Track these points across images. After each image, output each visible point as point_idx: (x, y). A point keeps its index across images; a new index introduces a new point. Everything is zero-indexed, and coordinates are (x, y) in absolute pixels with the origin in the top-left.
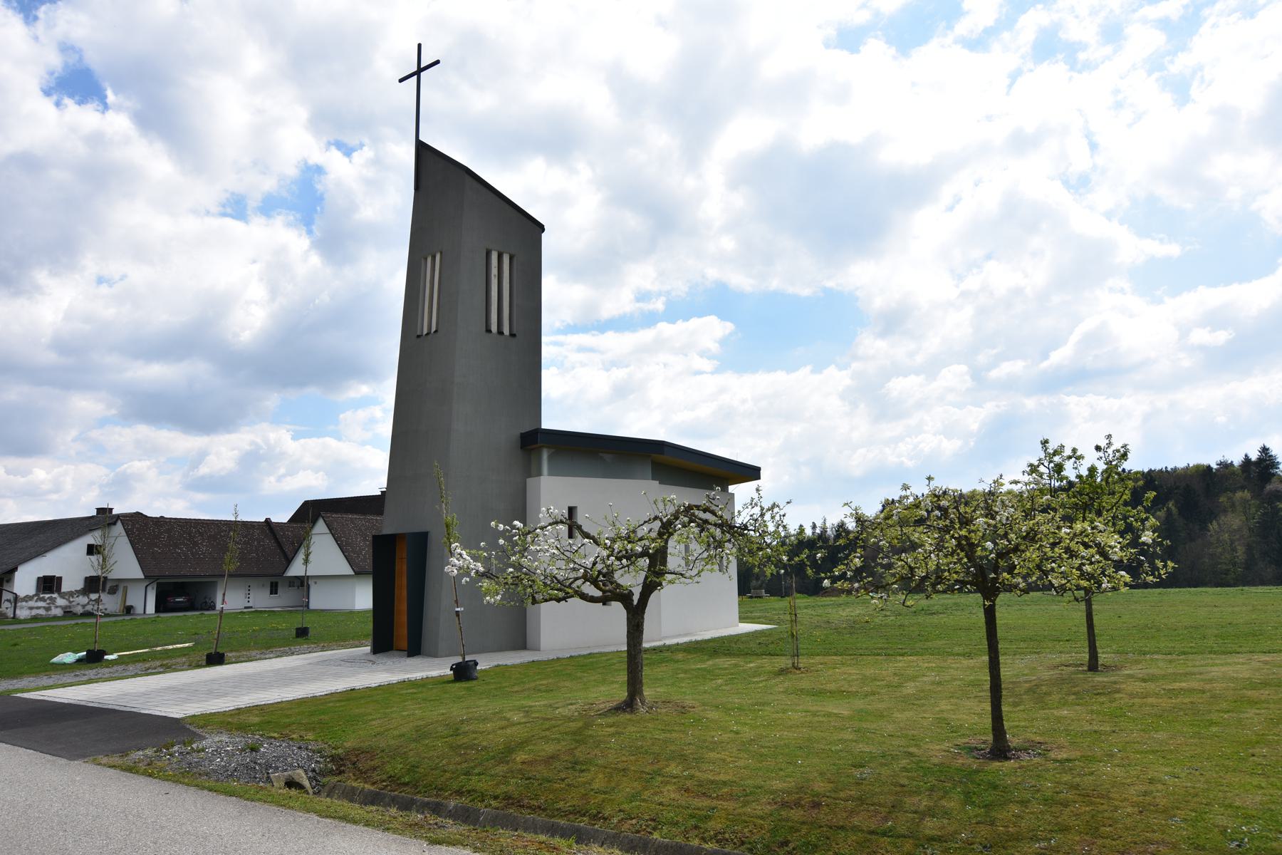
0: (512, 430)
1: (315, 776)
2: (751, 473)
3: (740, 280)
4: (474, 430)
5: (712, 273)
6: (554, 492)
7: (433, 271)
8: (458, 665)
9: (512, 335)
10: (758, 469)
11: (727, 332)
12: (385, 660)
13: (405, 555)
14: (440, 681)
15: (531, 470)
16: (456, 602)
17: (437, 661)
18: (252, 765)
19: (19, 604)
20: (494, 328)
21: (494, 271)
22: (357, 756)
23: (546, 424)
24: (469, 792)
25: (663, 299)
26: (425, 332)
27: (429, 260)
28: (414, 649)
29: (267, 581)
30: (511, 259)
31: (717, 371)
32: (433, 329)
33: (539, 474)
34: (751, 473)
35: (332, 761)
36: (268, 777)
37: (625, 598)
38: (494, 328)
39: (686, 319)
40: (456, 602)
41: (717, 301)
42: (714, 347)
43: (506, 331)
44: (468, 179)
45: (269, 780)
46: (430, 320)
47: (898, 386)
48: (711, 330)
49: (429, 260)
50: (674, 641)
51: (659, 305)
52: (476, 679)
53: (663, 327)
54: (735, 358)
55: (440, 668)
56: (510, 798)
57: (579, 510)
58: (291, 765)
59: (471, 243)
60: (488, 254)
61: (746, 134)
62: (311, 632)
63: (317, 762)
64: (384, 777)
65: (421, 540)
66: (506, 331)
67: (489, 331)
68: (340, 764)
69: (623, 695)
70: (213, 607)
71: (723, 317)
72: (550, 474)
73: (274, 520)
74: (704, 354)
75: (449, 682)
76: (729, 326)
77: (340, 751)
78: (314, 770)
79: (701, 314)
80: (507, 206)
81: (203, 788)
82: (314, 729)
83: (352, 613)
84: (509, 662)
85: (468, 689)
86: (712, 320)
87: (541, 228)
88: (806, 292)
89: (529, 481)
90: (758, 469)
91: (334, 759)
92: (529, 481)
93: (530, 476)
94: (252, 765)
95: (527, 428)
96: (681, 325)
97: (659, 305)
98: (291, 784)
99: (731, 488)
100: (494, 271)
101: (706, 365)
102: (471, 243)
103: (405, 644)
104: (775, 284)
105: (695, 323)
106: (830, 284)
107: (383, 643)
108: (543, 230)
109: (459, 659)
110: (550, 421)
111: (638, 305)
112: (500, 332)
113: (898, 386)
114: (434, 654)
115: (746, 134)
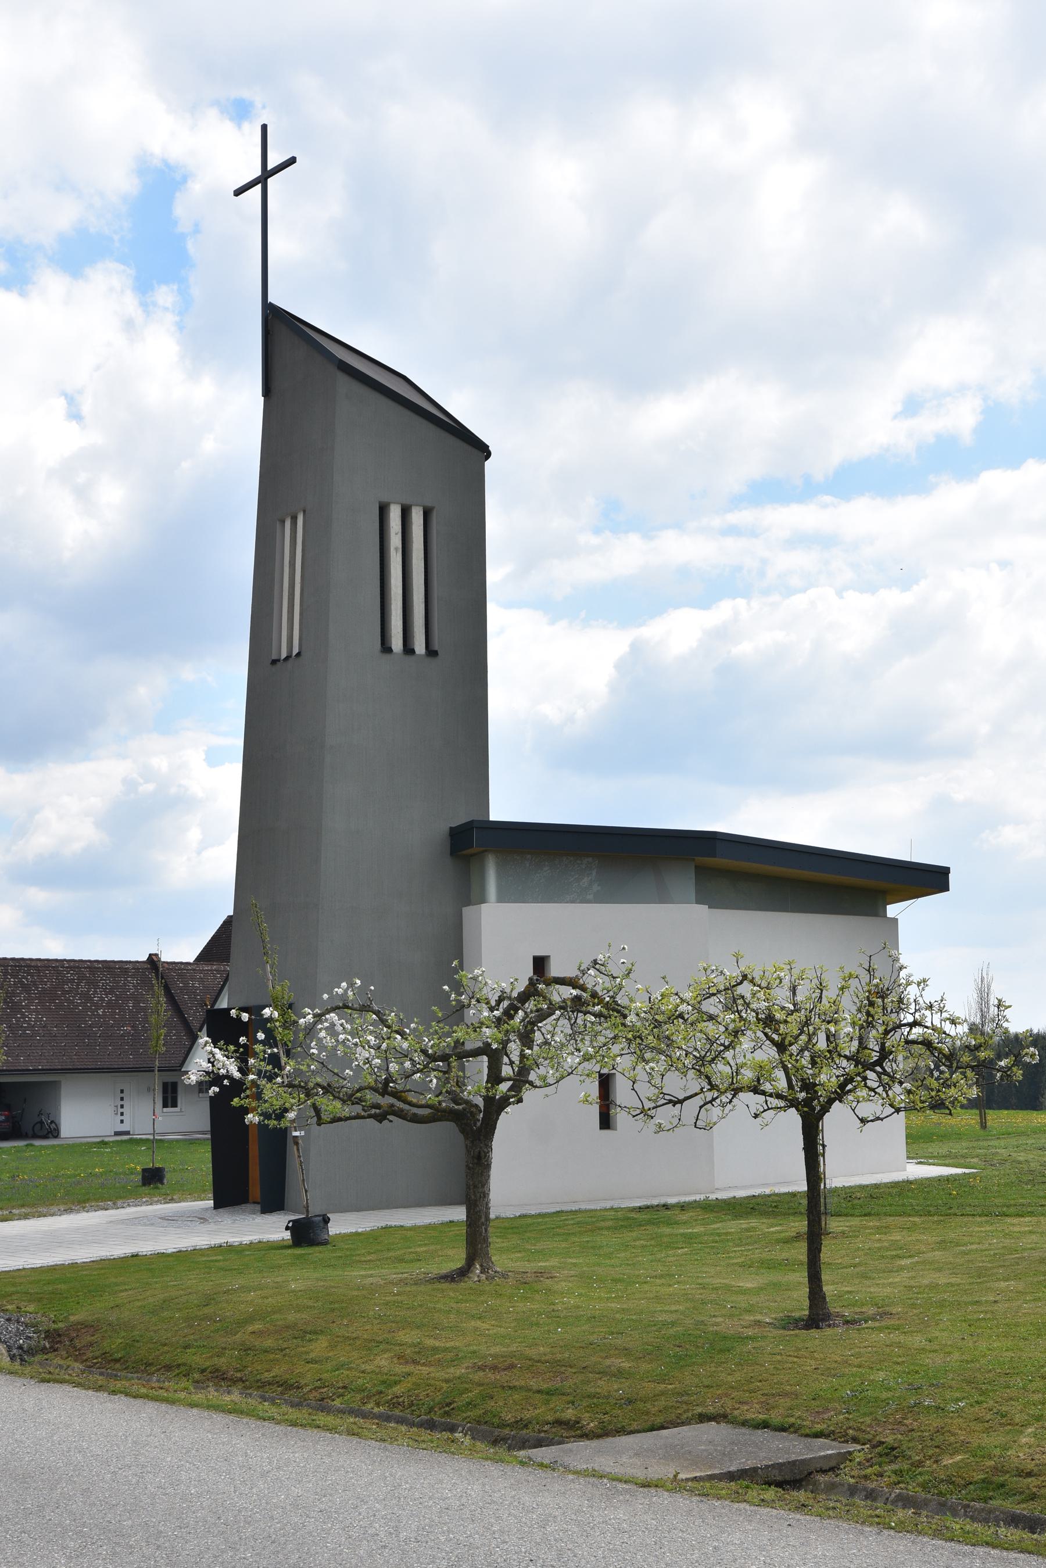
0: (424, 827)
4: (371, 827)
7: (293, 542)
10: (944, 872)
14: (280, 1246)
15: (469, 893)
26: (284, 655)
29: (157, 1081)
30: (427, 514)
32: (296, 651)
33: (483, 900)
46: (288, 637)
50: (691, 1198)
52: (325, 1243)
55: (273, 1229)
56: (217, 1370)
57: (552, 958)
59: (365, 487)
62: (168, 1176)
64: (98, 1353)
67: (386, 648)
68: (54, 1337)
70: (53, 1132)
72: (501, 899)
73: (166, 957)
75: (289, 1247)
77: (61, 1325)
78: (20, 1347)
82: (40, 1300)
83: (794, 1195)
84: (408, 1223)
87: (484, 451)
89: (466, 910)
90: (944, 872)
91: (48, 1334)
92: (466, 910)
93: (469, 903)
95: (460, 818)
102: (365, 487)
107: (229, 1193)
108: (488, 455)
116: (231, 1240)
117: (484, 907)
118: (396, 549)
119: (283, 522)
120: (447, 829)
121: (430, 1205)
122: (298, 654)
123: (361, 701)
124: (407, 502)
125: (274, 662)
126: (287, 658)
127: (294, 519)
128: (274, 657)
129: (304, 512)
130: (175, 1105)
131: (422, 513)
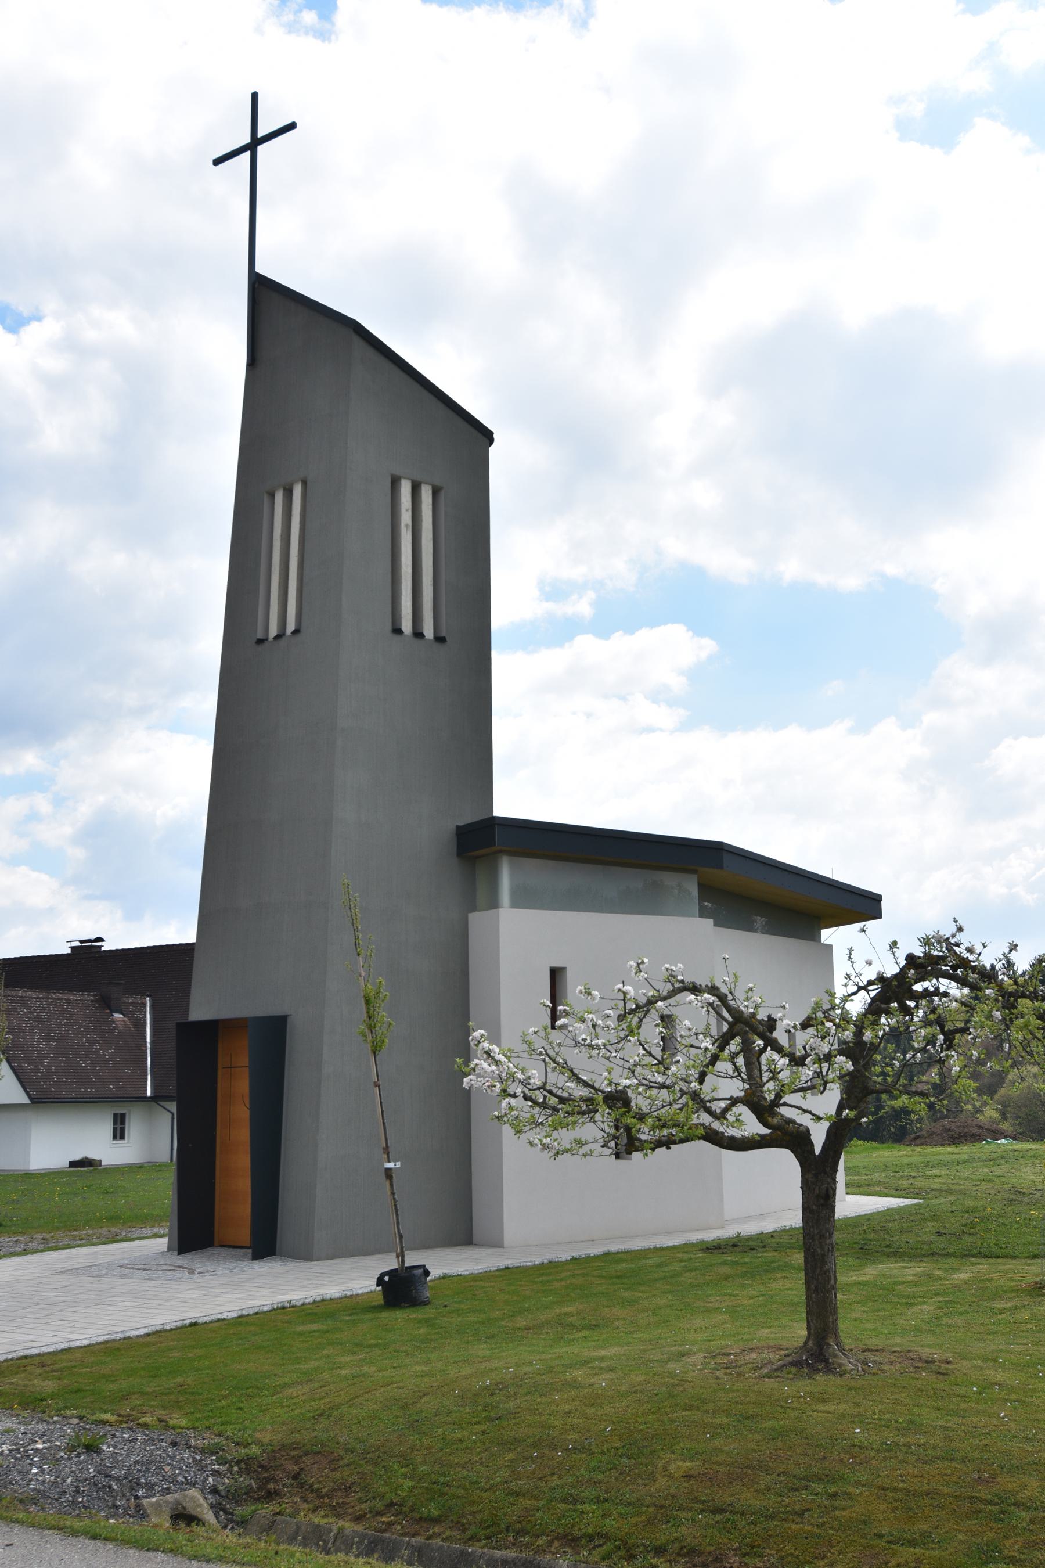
0: (430, 827)
1: (224, 1502)
2: (862, 906)
3: (725, 561)
4: (369, 821)
5: (676, 548)
6: (523, 936)
8: (391, 1273)
9: (439, 639)
11: (704, 655)
12: (209, 1266)
13: (244, 1060)
14: (349, 1307)
15: (477, 895)
16: (386, 1150)
17: (316, 1267)
18: (105, 1481)
19: (828, 1086)
20: (407, 626)
21: (406, 518)
22: (296, 1460)
23: (500, 810)
24: (591, 1538)
25: (591, 595)
26: (273, 632)
27: (279, 497)
28: (264, 1244)
30: (436, 492)
31: (685, 727)
32: (291, 627)
33: (494, 904)
34: (862, 906)
35: (248, 1471)
36: (139, 1507)
37: (793, 1138)
38: (407, 626)
39: (631, 629)
40: (386, 1150)
41: (681, 597)
42: (677, 683)
43: (429, 632)
44: (358, 342)
45: (140, 1513)
47: (1013, 755)
48: (672, 650)
49: (279, 497)
51: (583, 607)
52: (427, 1303)
53: (586, 644)
54: (712, 703)
57: (568, 970)
58: (174, 1482)
60: (395, 482)
61: (736, 298)
63: (216, 1473)
65: (272, 1035)
66: (429, 632)
67: (398, 631)
69: (799, 1332)
71: (698, 629)
72: (515, 904)
74: (658, 696)
76: (708, 646)
77: (255, 1450)
79: (654, 623)
80: (425, 394)
81: (74, 1533)
85: (427, 1322)
86: (676, 633)
87: (488, 436)
88: (851, 582)
89: (473, 917)
91: (247, 1465)
93: (474, 908)
94: (105, 1481)
95: (467, 818)
96: (620, 642)
97: (583, 607)
98: (183, 1517)
99: (827, 935)
100: (406, 518)
101: (664, 716)
103: (244, 1234)
104: (792, 569)
105: (644, 635)
106: (891, 569)
107: (196, 1233)
108: (491, 441)
109: (390, 1263)
110: (513, 799)
111: (549, 606)
112: (418, 634)
113: (1013, 755)
114: (305, 1254)
115: (736, 298)
116: (588, 1252)
117: (501, 910)
118: (407, 526)
119: (272, 496)
120: (454, 827)
121: (456, 1245)
122: (296, 632)
123: (364, 689)
124: (418, 478)
125: (260, 642)
126: (278, 637)
127: (289, 493)
128: (260, 636)
129: (304, 483)
130: (122, 1137)
131: (430, 492)
